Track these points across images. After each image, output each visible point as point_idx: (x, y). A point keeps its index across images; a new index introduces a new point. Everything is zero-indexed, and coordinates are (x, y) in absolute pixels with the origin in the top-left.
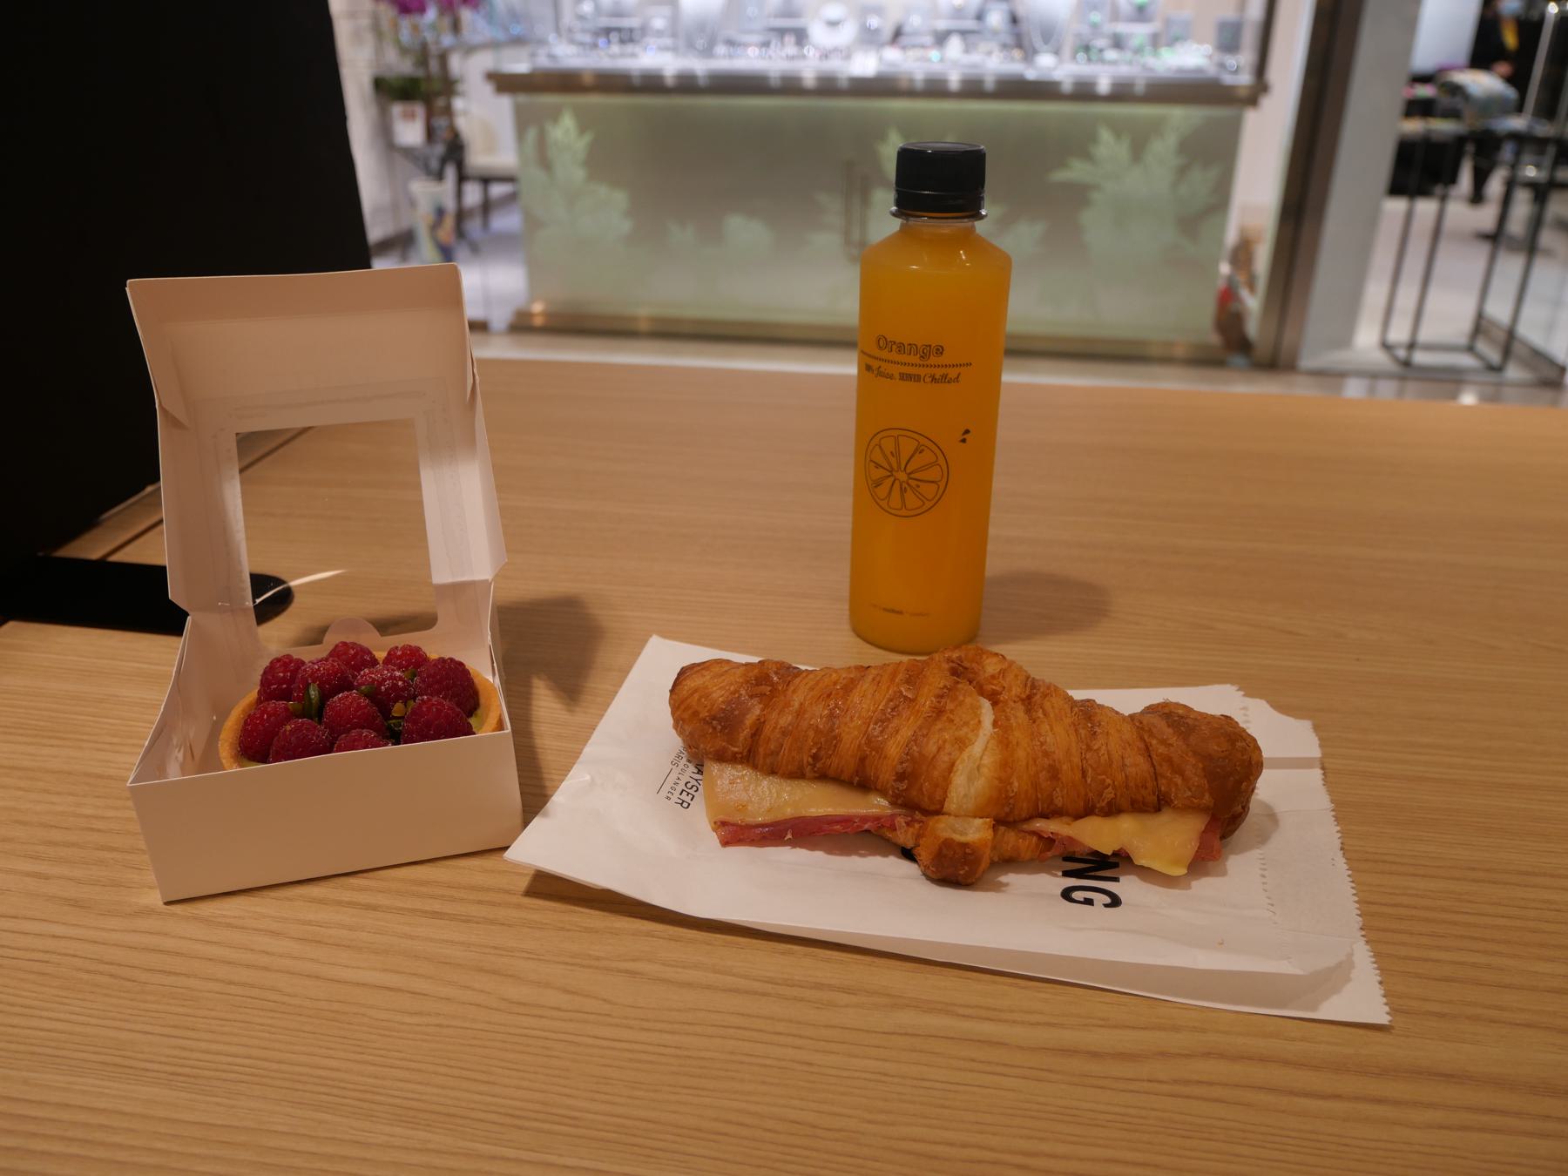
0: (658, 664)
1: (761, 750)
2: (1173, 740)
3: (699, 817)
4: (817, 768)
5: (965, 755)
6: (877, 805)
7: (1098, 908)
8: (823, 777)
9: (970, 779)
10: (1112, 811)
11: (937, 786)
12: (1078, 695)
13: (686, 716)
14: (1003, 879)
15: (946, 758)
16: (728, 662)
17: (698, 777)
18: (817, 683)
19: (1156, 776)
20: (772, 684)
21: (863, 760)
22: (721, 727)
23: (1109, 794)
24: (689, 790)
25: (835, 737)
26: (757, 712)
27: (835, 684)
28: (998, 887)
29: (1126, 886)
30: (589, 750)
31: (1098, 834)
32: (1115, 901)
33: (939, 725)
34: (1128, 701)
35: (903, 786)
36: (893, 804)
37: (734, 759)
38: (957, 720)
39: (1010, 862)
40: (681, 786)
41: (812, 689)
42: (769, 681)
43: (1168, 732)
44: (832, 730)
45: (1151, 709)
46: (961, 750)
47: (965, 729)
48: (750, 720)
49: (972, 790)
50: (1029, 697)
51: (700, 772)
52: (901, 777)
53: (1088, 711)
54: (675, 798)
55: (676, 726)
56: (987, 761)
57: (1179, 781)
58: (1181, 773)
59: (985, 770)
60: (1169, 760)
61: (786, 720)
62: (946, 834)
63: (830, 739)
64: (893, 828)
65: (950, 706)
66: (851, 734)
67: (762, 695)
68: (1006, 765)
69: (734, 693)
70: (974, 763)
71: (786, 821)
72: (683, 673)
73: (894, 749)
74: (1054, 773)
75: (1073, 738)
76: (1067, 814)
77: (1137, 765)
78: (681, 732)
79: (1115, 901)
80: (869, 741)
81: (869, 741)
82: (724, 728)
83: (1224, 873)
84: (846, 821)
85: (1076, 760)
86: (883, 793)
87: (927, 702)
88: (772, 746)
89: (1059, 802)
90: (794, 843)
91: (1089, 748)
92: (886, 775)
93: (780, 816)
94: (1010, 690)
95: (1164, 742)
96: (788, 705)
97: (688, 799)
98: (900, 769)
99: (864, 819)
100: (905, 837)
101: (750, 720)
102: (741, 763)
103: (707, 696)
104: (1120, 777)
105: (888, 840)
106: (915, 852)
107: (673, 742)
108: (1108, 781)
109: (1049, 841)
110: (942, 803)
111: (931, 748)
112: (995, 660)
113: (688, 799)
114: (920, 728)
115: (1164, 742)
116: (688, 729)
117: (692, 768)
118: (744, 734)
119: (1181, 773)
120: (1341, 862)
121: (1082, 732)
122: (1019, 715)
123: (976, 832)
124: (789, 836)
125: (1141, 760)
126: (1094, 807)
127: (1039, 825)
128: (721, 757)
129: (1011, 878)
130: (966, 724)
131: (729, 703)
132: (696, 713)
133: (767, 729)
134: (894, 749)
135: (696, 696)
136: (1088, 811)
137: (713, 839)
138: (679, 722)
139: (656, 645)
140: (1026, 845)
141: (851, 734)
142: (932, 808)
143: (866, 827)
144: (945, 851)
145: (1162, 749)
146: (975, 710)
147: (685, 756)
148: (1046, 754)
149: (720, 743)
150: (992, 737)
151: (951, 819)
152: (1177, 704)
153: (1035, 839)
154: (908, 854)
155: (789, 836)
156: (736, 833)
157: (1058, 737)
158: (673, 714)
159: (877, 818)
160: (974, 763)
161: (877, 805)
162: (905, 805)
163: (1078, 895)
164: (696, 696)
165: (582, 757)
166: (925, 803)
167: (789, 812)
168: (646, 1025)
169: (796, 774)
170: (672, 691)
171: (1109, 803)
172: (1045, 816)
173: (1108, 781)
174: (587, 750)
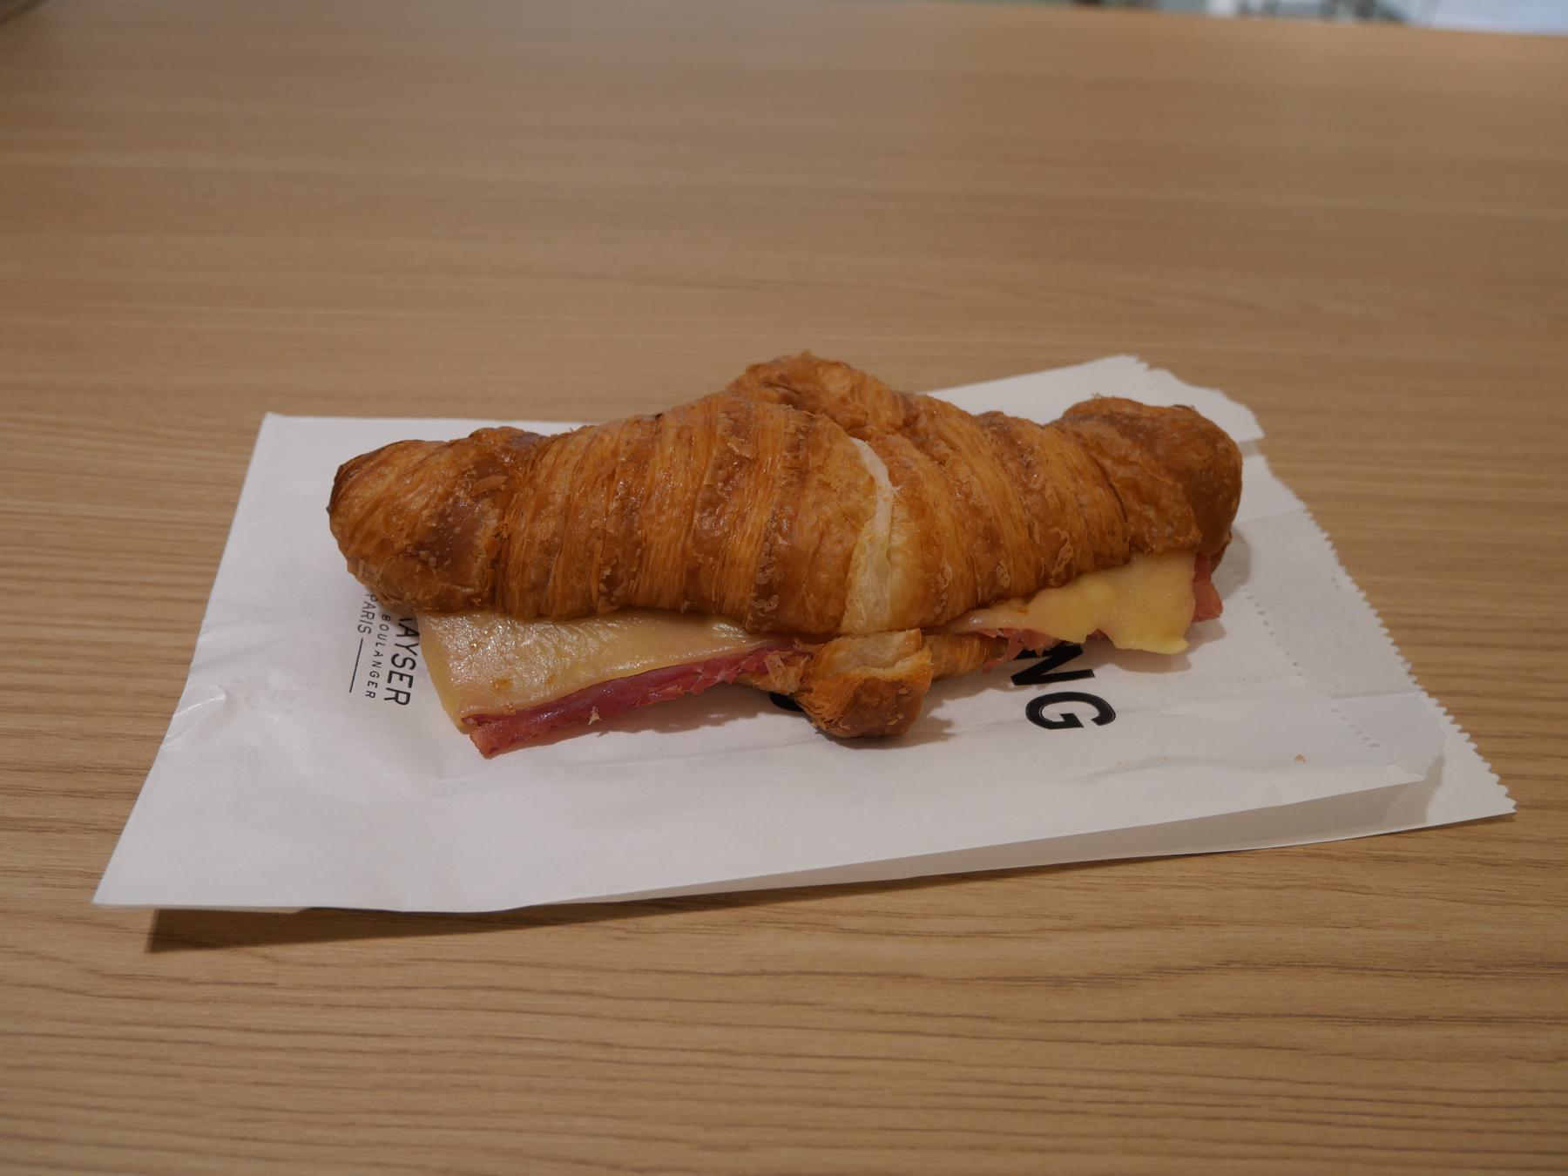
0: (295, 464)
1: (514, 585)
2: (1136, 455)
3: (431, 713)
4: (619, 599)
5: (864, 538)
6: (723, 639)
7: (1090, 731)
8: (627, 608)
9: (882, 574)
10: (1069, 577)
11: (828, 596)
12: (974, 398)
13: (369, 549)
14: (939, 713)
15: (838, 549)
16: (417, 444)
17: (408, 641)
18: (585, 456)
19: (1125, 513)
20: (505, 471)
21: (693, 573)
22: (429, 556)
23: (1066, 553)
24: (401, 668)
25: (638, 544)
26: (493, 523)
27: (615, 453)
28: (938, 731)
29: (1106, 681)
30: (207, 641)
31: (1060, 615)
32: (1105, 715)
33: (811, 498)
34: (1039, 397)
35: (774, 603)
36: (753, 633)
37: (467, 607)
38: (835, 483)
39: (946, 682)
40: (387, 666)
41: (579, 468)
42: (498, 465)
43: (1124, 444)
44: (631, 532)
45: (1079, 413)
46: (856, 530)
47: (855, 496)
48: (483, 538)
49: (887, 595)
50: (907, 423)
51: (411, 632)
52: (765, 591)
53: (999, 428)
54: (382, 692)
55: (354, 567)
56: (898, 540)
57: (1151, 513)
58: (1153, 501)
59: (898, 557)
60: (1135, 487)
61: (545, 529)
62: (859, 673)
63: (632, 548)
64: (763, 671)
65: (814, 461)
66: (664, 533)
67: (493, 492)
68: (928, 542)
69: (444, 497)
70: (879, 548)
71: (583, 693)
72: (345, 477)
73: (744, 548)
74: (992, 539)
75: (1005, 478)
76: (1016, 596)
77: (1094, 501)
78: (365, 578)
79: (1105, 715)
80: (698, 543)
81: (698, 543)
82: (441, 559)
83: (1220, 634)
84: (682, 674)
85: (1016, 511)
86: (736, 618)
87: (776, 463)
88: (532, 575)
89: (1005, 581)
90: (603, 726)
91: (1028, 491)
92: (738, 591)
93: (570, 687)
94: (877, 416)
95: (1122, 461)
96: (543, 503)
97: (402, 685)
98: (761, 579)
99: (712, 665)
100: (783, 680)
101: (483, 538)
102: (481, 609)
103: (401, 511)
104: (1079, 525)
105: (758, 691)
106: (803, 700)
107: (350, 592)
108: (1064, 534)
109: (994, 643)
110: (838, 621)
111: (806, 536)
112: (837, 373)
113: (402, 685)
114: (781, 506)
115: (1122, 461)
116: (377, 571)
117: (394, 631)
118: (478, 565)
119: (1153, 501)
120: (1346, 581)
121: (1010, 465)
122: (904, 446)
123: (902, 659)
124: (595, 717)
125: (1100, 492)
126: (1047, 576)
127: (977, 621)
128: (446, 607)
129: (950, 709)
130: (852, 486)
131: (442, 516)
132: (385, 544)
133: (517, 548)
134: (744, 548)
135: (380, 515)
136: (1043, 582)
137: (465, 747)
138: (357, 562)
139: (276, 431)
140: (966, 656)
141: (664, 533)
142: (822, 629)
143: (719, 678)
144: (865, 699)
145: (1121, 472)
146: (854, 458)
147: (377, 610)
148: (977, 511)
149: (439, 585)
150: (897, 501)
151: (858, 643)
152: (1115, 400)
153: (976, 643)
154: (786, 704)
155: (595, 717)
156: (502, 729)
157: (983, 476)
158: (344, 548)
159: (733, 662)
160: (879, 548)
161: (723, 639)
162: (772, 633)
163: (1052, 712)
164: (380, 515)
165: (198, 658)
166: (811, 624)
167: (585, 677)
168: (334, 996)
169: (582, 613)
170: (333, 509)
171: (1068, 567)
172: (984, 605)
173: (1064, 534)
174: (205, 640)
